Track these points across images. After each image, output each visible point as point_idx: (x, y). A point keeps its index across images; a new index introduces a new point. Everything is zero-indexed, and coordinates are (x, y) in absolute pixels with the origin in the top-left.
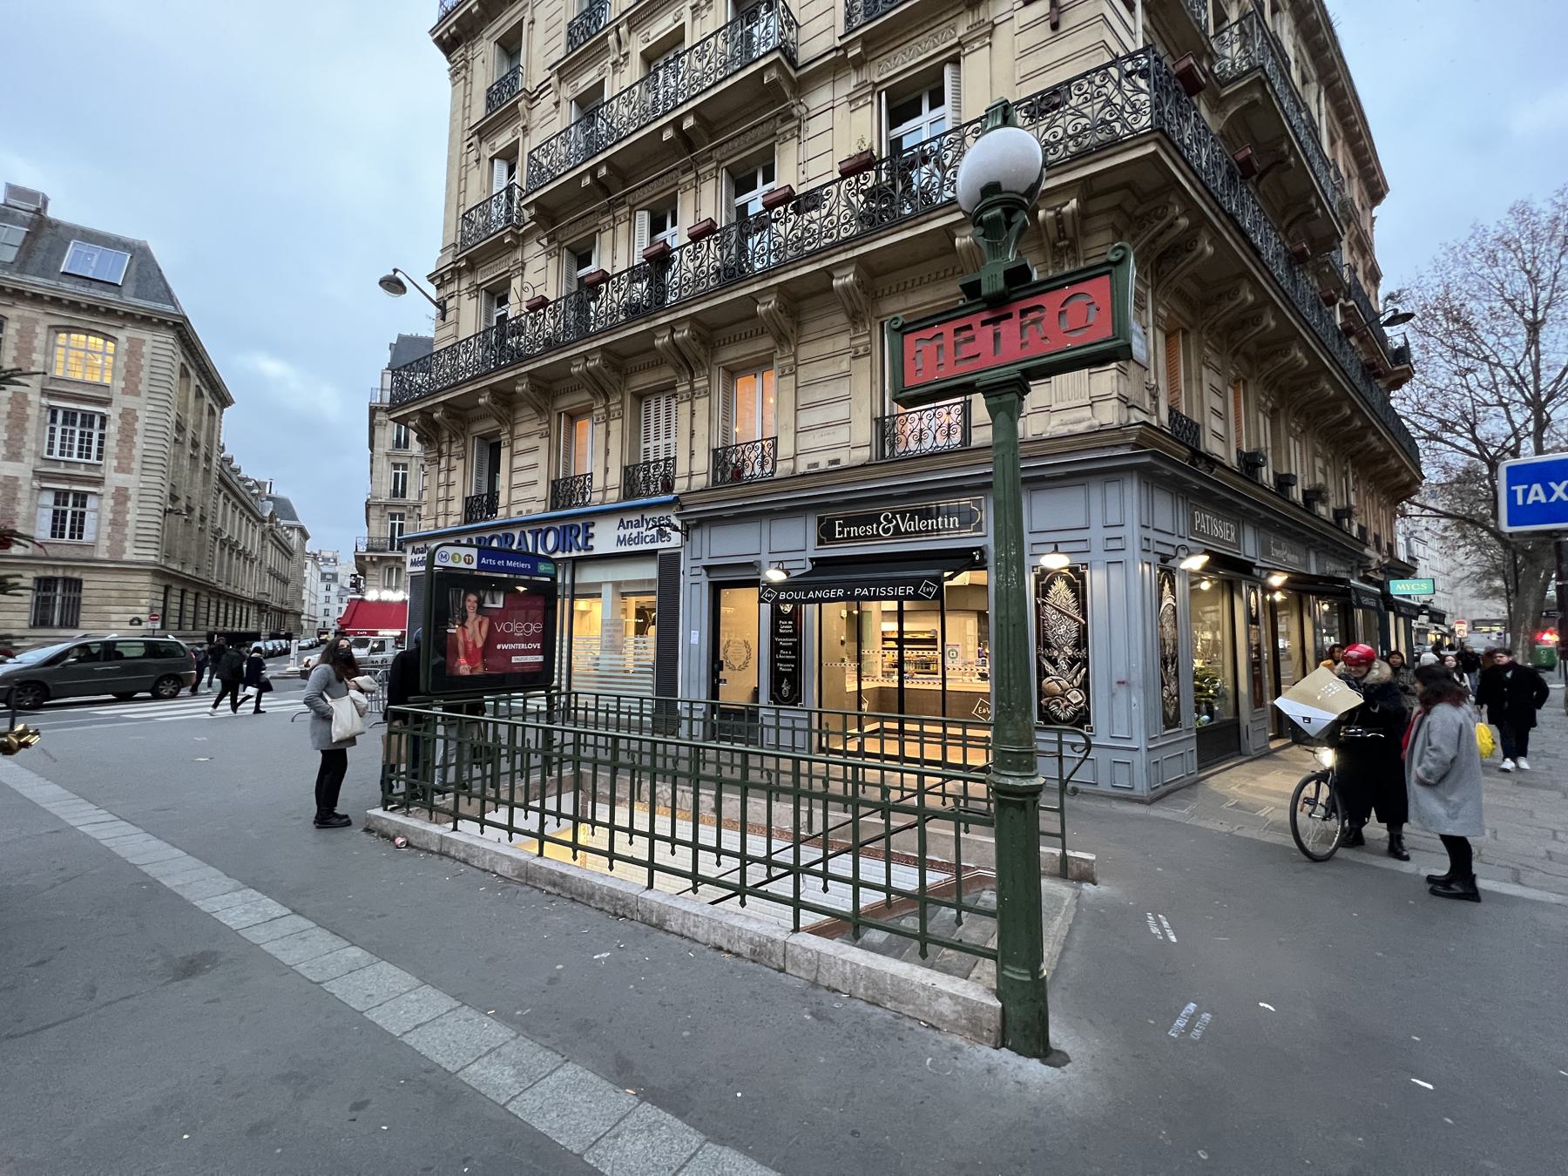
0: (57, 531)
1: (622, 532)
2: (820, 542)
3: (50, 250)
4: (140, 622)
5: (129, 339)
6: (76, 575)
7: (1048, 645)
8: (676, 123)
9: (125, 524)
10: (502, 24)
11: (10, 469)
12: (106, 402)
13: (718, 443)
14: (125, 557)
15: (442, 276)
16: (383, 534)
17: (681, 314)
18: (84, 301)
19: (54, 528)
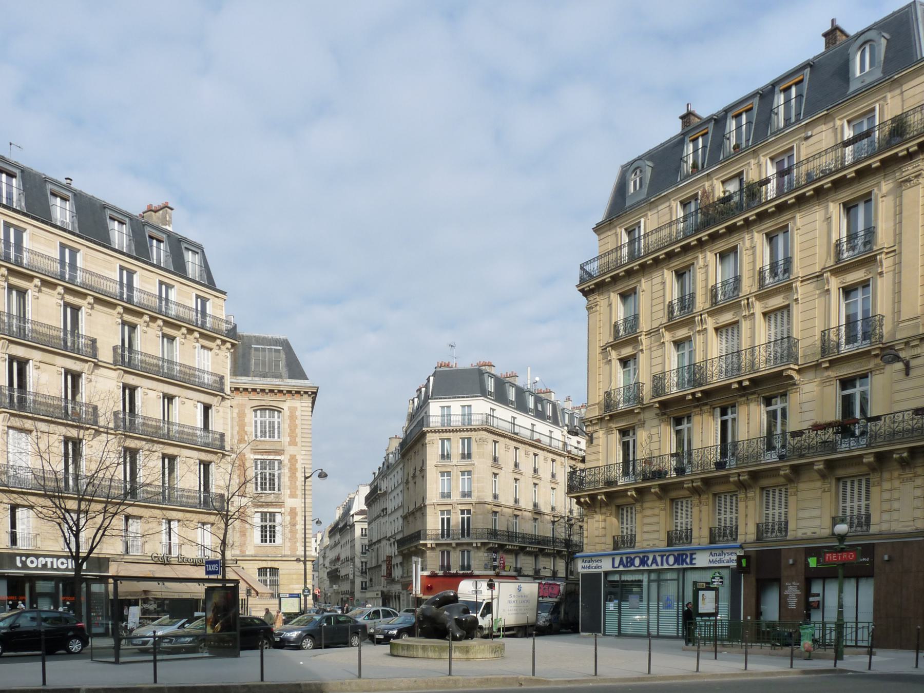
1: (711, 558)
8: (740, 383)
10: (624, 286)
13: (657, 370)
15: (591, 421)
18: (267, 388)
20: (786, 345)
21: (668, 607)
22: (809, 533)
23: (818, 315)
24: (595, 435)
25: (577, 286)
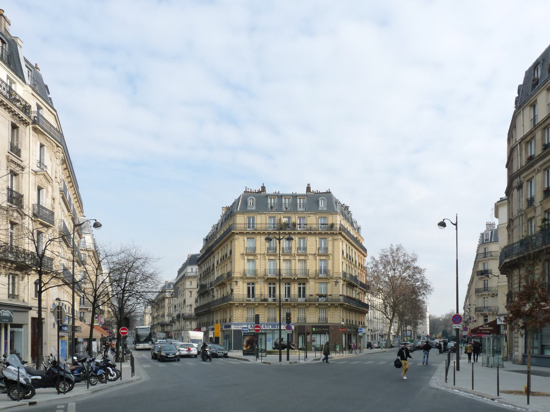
20: (306, 272)
21: (269, 341)
23: (313, 265)
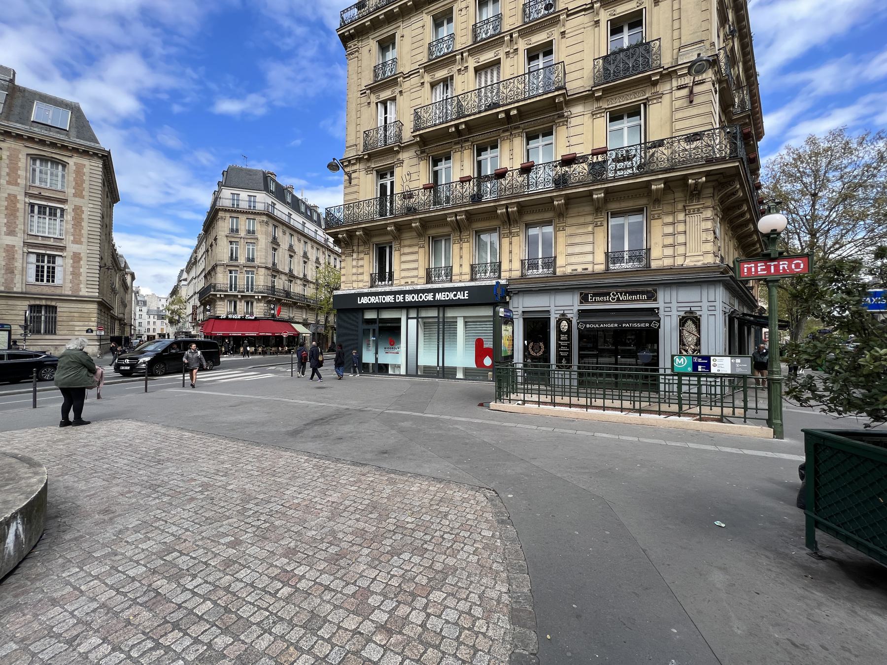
0: (39, 277)
2: (581, 303)
3: (22, 107)
4: (92, 331)
5: (75, 164)
6: (53, 304)
7: (684, 345)
9: (80, 274)
10: (384, 32)
11: (9, 240)
12: (64, 201)
14: (81, 294)
15: (349, 161)
16: (225, 282)
17: (513, 201)
18: (48, 140)
19: (37, 275)
22: (580, 269)
24: (353, 175)
25: (338, 30)
